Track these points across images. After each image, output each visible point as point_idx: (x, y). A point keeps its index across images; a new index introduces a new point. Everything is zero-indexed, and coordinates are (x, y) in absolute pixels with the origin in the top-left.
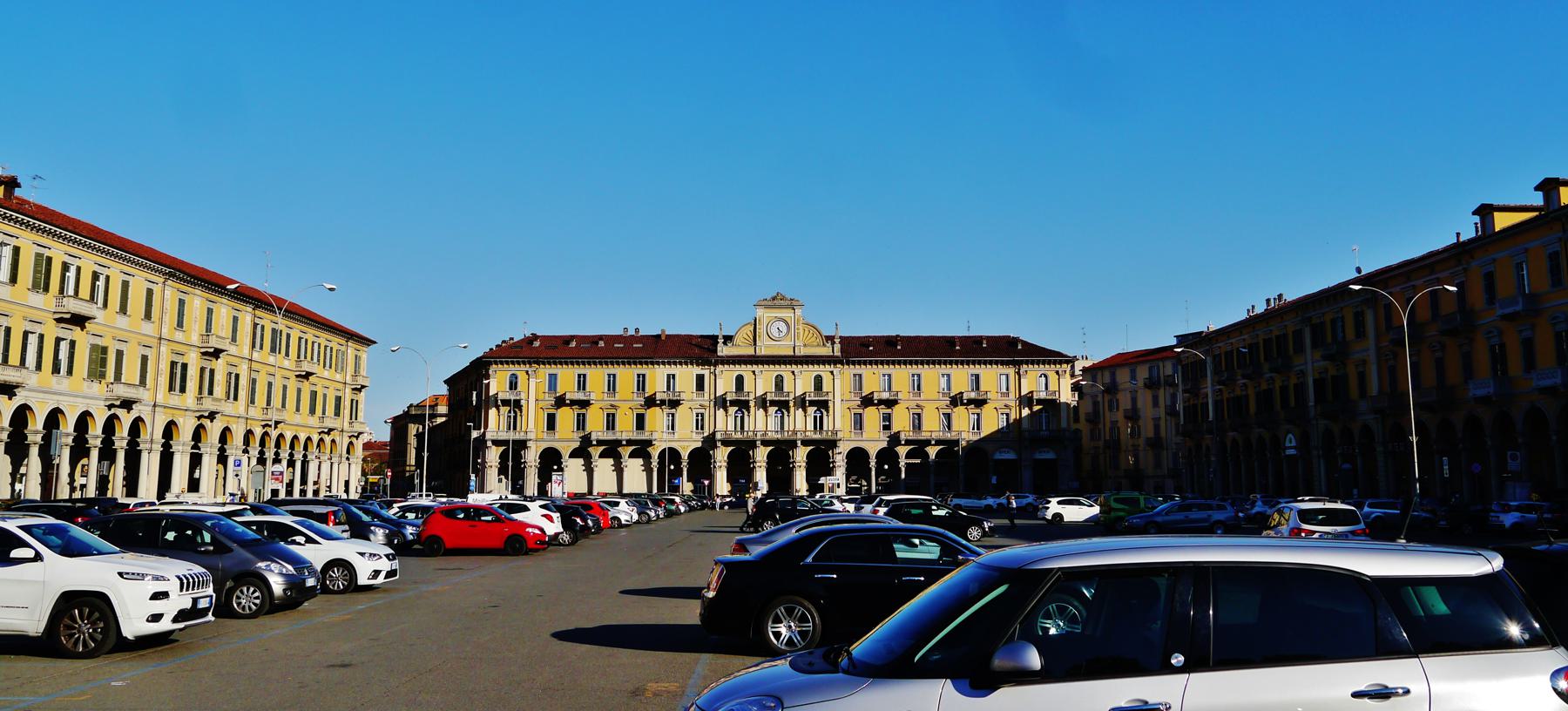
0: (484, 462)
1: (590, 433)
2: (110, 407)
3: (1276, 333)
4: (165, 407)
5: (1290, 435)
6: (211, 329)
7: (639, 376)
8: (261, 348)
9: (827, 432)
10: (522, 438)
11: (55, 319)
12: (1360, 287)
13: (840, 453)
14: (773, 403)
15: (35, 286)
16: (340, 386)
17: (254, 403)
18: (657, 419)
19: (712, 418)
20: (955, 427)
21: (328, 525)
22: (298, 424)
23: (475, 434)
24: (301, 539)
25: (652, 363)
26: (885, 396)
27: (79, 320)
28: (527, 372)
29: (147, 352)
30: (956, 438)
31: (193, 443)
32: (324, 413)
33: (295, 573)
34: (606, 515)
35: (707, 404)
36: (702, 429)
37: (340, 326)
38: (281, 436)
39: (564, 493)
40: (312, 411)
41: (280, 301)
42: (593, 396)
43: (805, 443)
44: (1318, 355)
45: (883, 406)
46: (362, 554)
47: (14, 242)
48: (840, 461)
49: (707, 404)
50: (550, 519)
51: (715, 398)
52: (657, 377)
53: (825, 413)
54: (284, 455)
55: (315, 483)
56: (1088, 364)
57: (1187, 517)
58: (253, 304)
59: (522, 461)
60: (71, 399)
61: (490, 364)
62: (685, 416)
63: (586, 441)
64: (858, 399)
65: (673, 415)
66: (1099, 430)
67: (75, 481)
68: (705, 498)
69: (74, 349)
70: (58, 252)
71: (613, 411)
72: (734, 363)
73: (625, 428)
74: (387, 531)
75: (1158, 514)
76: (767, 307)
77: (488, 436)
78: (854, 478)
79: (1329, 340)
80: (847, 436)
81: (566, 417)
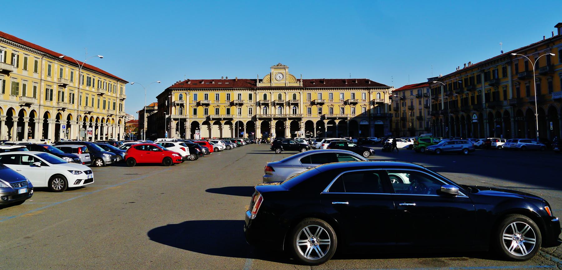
0: (171, 126)
1: (210, 116)
2: (21, 106)
3: (469, 76)
5: (475, 115)
6: (62, 76)
7: (227, 94)
8: (83, 84)
9: (298, 115)
10: (184, 118)
12: (516, 54)
13: (303, 122)
14: (278, 104)
16: (115, 99)
18: (234, 110)
19: (255, 110)
20: (345, 112)
21: (78, 153)
22: (98, 112)
23: (167, 116)
24: (38, 164)
25: (232, 90)
26: (319, 101)
28: (186, 93)
29: (36, 85)
30: (346, 117)
31: (56, 120)
32: (109, 108)
33: (10, 186)
34: (212, 147)
35: (253, 104)
36: (251, 114)
38: (92, 117)
39: (200, 138)
40: (104, 108)
41: (81, 63)
42: (210, 102)
43: (290, 119)
44: (487, 84)
45: (319, 105)
46: (71, 171)
48: (303, 125)
49: (253, 104)
50: (184, 149)
51: (256, 102)
52: (234, 95)
53: (297, 108)
54: (94, 124)
55: (106, 135)
56: (394, 89)
57: (453, 147)
61: (172, 90)
62: (245, 109)
63: (208, 118)
64: (309, 102)
65: (240, 109)
66: (399, 113)
67: (10, 134)
68: (252, 139)
71: (218, 107)
72: (263, 89)
73: (223, 114)
75: (441, 145)
76: (275, 68)
77: (172, 117)
78: (308, 131)
79: (492, 78)
80: (305, 116)
81: (201, 110)
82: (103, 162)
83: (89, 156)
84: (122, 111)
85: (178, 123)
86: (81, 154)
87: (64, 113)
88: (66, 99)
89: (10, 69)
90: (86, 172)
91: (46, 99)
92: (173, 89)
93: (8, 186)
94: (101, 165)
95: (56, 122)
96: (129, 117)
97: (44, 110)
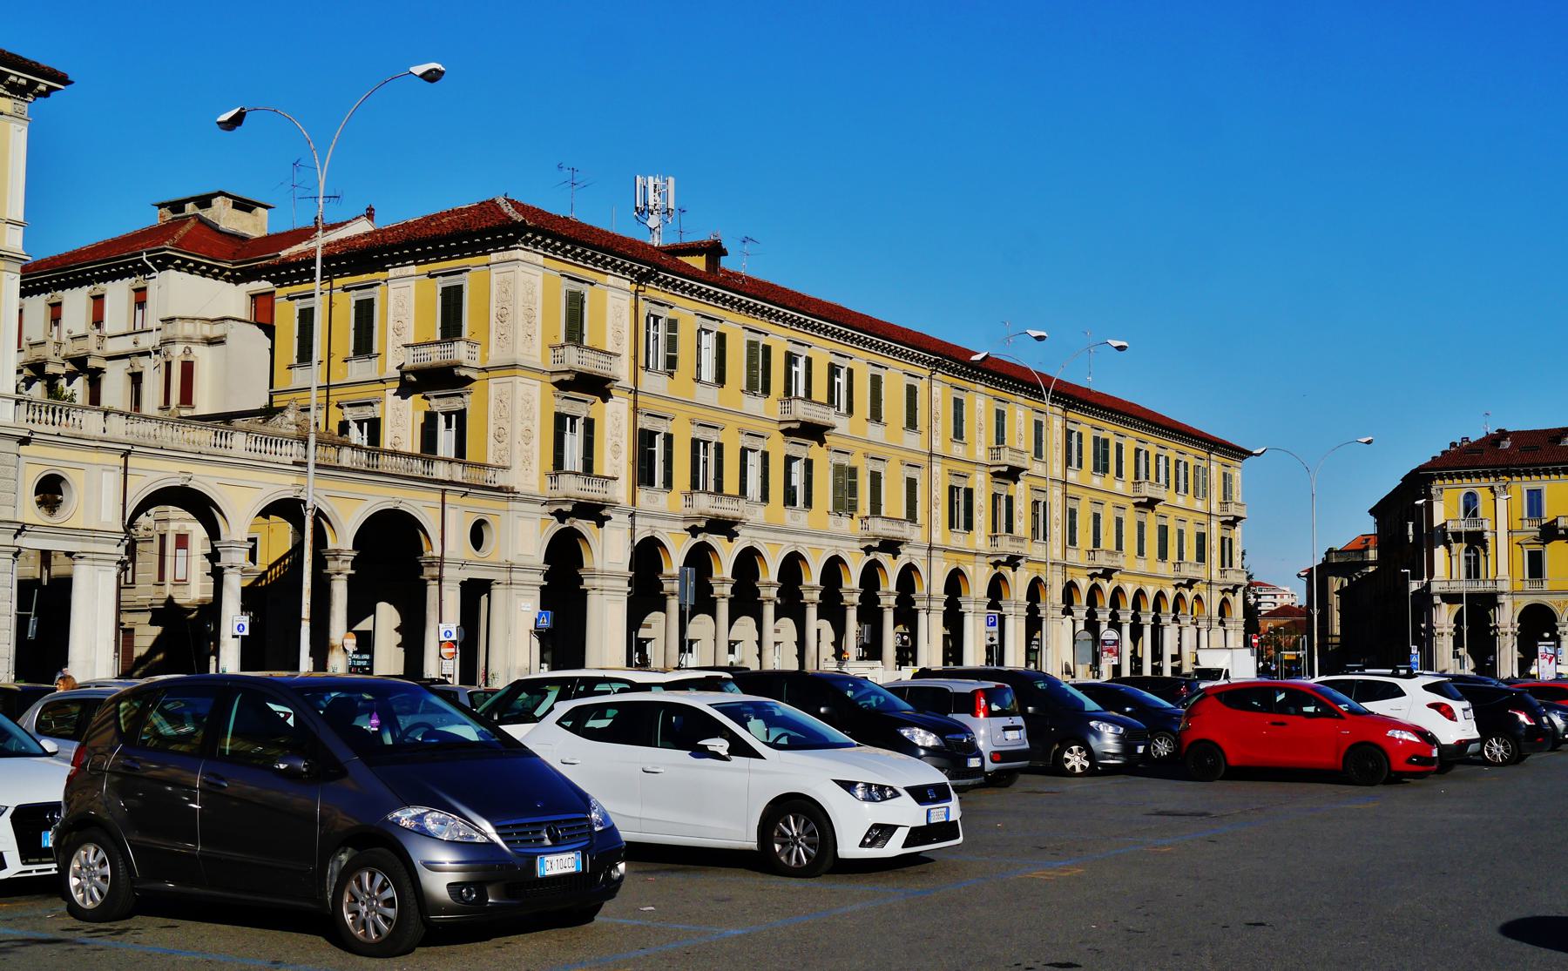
0: (1431, 627)
2: (868, 550)
4: (945, 550)
11: (781, 431)
15: (751, 387)
16: (1204, 519)
17: (1074, 544)
21: (975, 714)
23: (1414, 586)
24: (720, 745)
27: (814, 432)
29: (914, 473)
32: (1181, 556)
37: (1178, 423)
38: (1118, 591)
40: (1163, 555)
46: (849, 786)
47: (717, 327)
50: (1449, 713)
54: (1126, 617)
55: (1174, 658)
58: (1063, 402)
59: (1492, 625)
60: (814, 540)
61: (1432, 479)
69: (811, 472)
70: (779, 339)
74: (1122, 730)
77: (1435, 588)
82: (1091, 755)
83: (1018, 728)
84: (1231, 565)
85: (1460, 611)
86: (986, 716)
87: (1015, 577)
88: (1022, 525)
89: (826, 420)
90: (921, 794)
91: (951, 526)
92: (1435, 473)
93: (485, 835)
94: (1082, 767)
95: (989, 608)
96: (1275, 596)
97: (1027, 573)
